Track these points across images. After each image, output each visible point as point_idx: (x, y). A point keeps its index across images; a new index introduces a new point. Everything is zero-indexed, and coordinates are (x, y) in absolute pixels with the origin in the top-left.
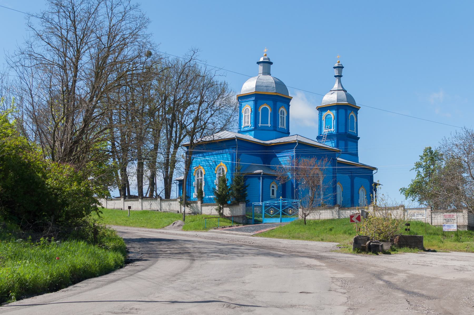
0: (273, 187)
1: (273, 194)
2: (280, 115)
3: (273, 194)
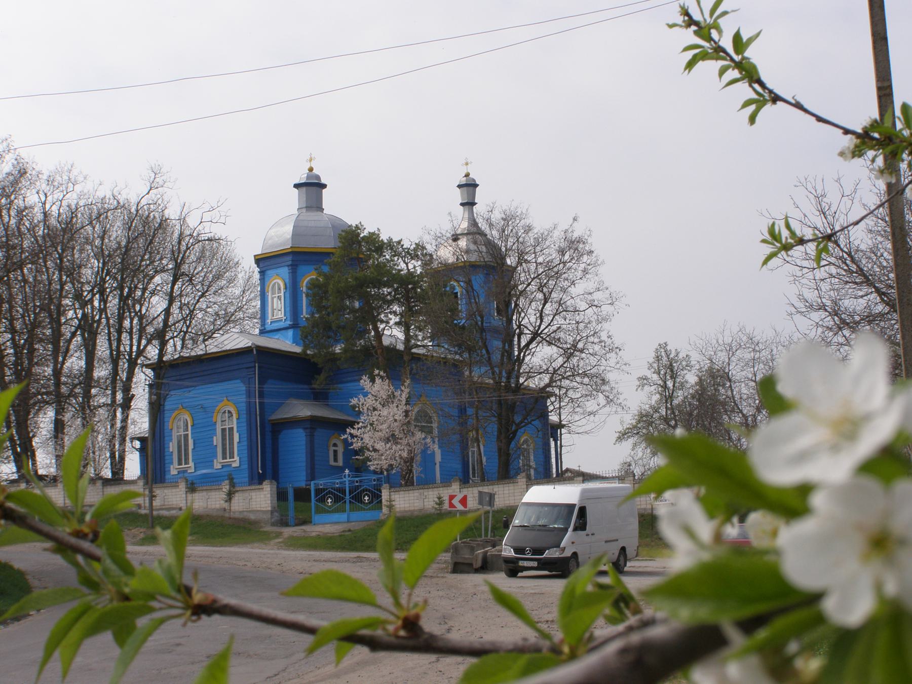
0: (335, 445)
1: (336, 460)
2: (190, 432)
3: (336, 460)
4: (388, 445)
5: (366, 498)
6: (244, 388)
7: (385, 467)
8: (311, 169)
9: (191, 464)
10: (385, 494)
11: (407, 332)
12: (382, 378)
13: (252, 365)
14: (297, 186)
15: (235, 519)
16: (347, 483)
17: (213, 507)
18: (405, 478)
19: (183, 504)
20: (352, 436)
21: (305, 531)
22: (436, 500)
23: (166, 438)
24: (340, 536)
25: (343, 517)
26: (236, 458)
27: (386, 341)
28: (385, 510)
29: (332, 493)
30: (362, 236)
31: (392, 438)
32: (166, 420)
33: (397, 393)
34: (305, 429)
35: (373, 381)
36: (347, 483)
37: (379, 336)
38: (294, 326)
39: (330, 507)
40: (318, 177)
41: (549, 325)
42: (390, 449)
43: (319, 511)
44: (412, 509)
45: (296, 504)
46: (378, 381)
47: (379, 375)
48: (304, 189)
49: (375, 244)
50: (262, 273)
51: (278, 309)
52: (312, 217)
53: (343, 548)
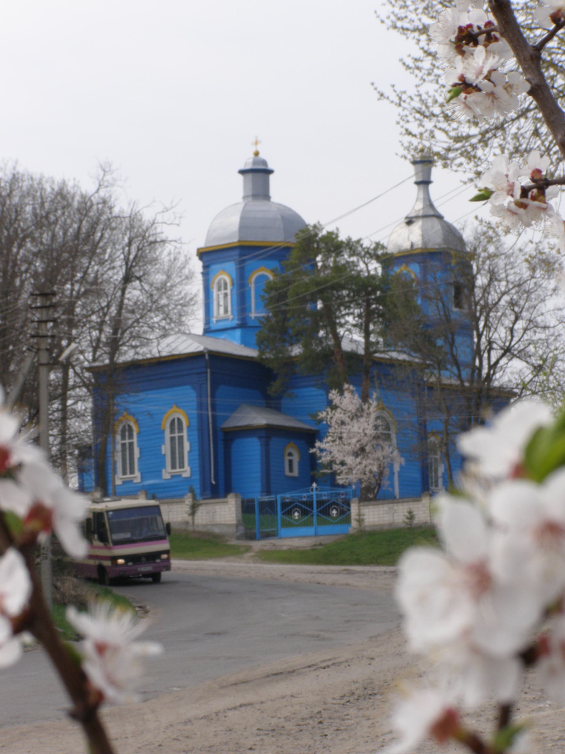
0: (290, 454)
1: (291, 470)
3: (291, 470)
4: (358, 460)
5: (334, 512)
7: (355, 481)
8: (257, 154)
9: (137, 474)
10: (354, 508)
11: (367, 336)
12: (352, 392)
14: (242, 172)
15: (199, 533)
16: (315, 497)
18: (372, 492)
20: (322, 450)
21: (274, 545)
22: (407, 514)
24: (313, 550)
25: (310, 530)
26: (187, 468)
27: (346, 346)
28: (354, 524)
29: (299, 507)
30: (320, 235)
31: (361, 451)
33: (365, 407)
34: (260, 438)
35: (341, 393)
36: (315, 497)
37: (338, 339)
38: (243, 325)
39: (296, 521)
40: (264, 163)
41: (520, 340)
42: (360, 463)
43: (286, 525)
44: (381, 523)
45: (258, 519)
46: (346, 394)
47: (348, 389)
48: (250, 176)
49: (333, 245)
50: (206, 267)
51: (224, 308)
52: (259, 206)
53: (318, 562)
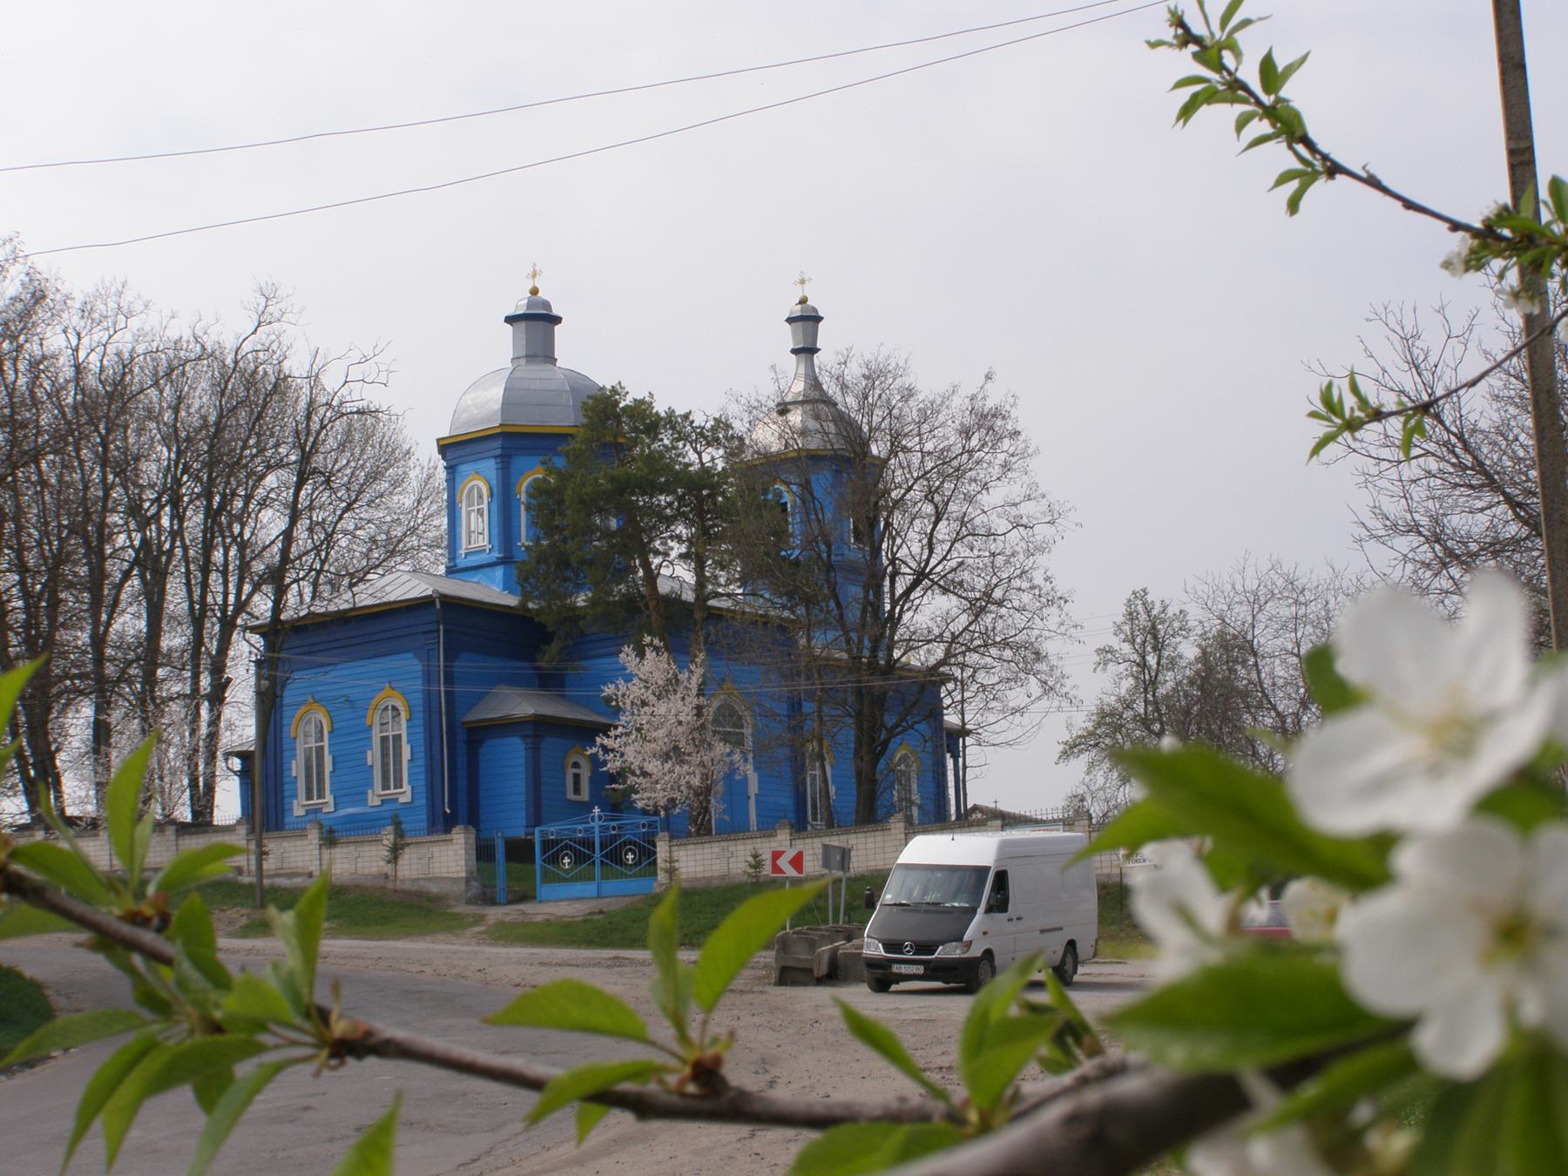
0: (576, 765)
1: (577, 791)
2: (326, 743)
3: (577, 791)
4: (668, 766)
5: (630, 856)
6: (420, 668)
7: (662, 803)
8: (534, 291)
9: (329, 798)
10: (662, 849)
11: (699, 571)
12: (657, 649)
13: (434, 627)
14: (510, 320)
15: (404, 892)
16: (597, 830)
17: (367, 871)
18: (697, 822)
19: (314, 867)
20: (606, 750)
21: (524, 913)
22: (750, 859)
23: (286, 754)
24: (585, 921)
25: (590, 888)
26: (406, 787)
27: (664, 587)
28: (662, 877)
29: (571, 848)
30: (622, 405)
31: (673, 753)
32: (285, 721)
33: (683, 676)
34: (524, 737)
35: (641, 654)
36: (597, 830)
37: (651, 577)
38: (506, 561)
39: (567, 871)
40: (547, 305)
41: (944, 558)
42: (671, 771)
43: (549, 878)
44: (708, 874)
45: (509, 867)
46: (650, 654)
47: (651, 644)
48: (522, 325)
49: (645, 419)
50: (451, 469)
51: (478, 531)
52: (537, 373)
53: (590, 943)
